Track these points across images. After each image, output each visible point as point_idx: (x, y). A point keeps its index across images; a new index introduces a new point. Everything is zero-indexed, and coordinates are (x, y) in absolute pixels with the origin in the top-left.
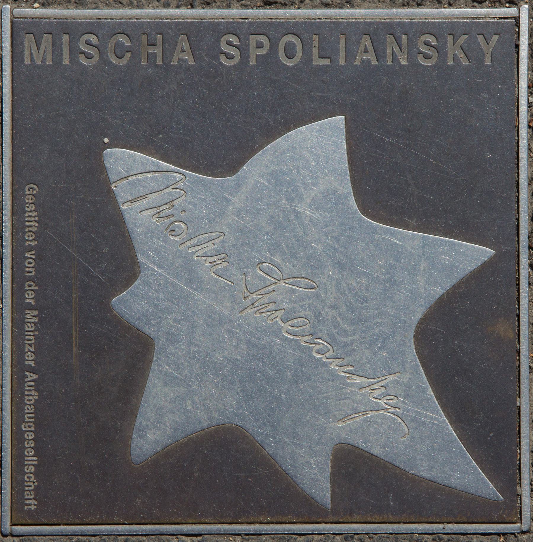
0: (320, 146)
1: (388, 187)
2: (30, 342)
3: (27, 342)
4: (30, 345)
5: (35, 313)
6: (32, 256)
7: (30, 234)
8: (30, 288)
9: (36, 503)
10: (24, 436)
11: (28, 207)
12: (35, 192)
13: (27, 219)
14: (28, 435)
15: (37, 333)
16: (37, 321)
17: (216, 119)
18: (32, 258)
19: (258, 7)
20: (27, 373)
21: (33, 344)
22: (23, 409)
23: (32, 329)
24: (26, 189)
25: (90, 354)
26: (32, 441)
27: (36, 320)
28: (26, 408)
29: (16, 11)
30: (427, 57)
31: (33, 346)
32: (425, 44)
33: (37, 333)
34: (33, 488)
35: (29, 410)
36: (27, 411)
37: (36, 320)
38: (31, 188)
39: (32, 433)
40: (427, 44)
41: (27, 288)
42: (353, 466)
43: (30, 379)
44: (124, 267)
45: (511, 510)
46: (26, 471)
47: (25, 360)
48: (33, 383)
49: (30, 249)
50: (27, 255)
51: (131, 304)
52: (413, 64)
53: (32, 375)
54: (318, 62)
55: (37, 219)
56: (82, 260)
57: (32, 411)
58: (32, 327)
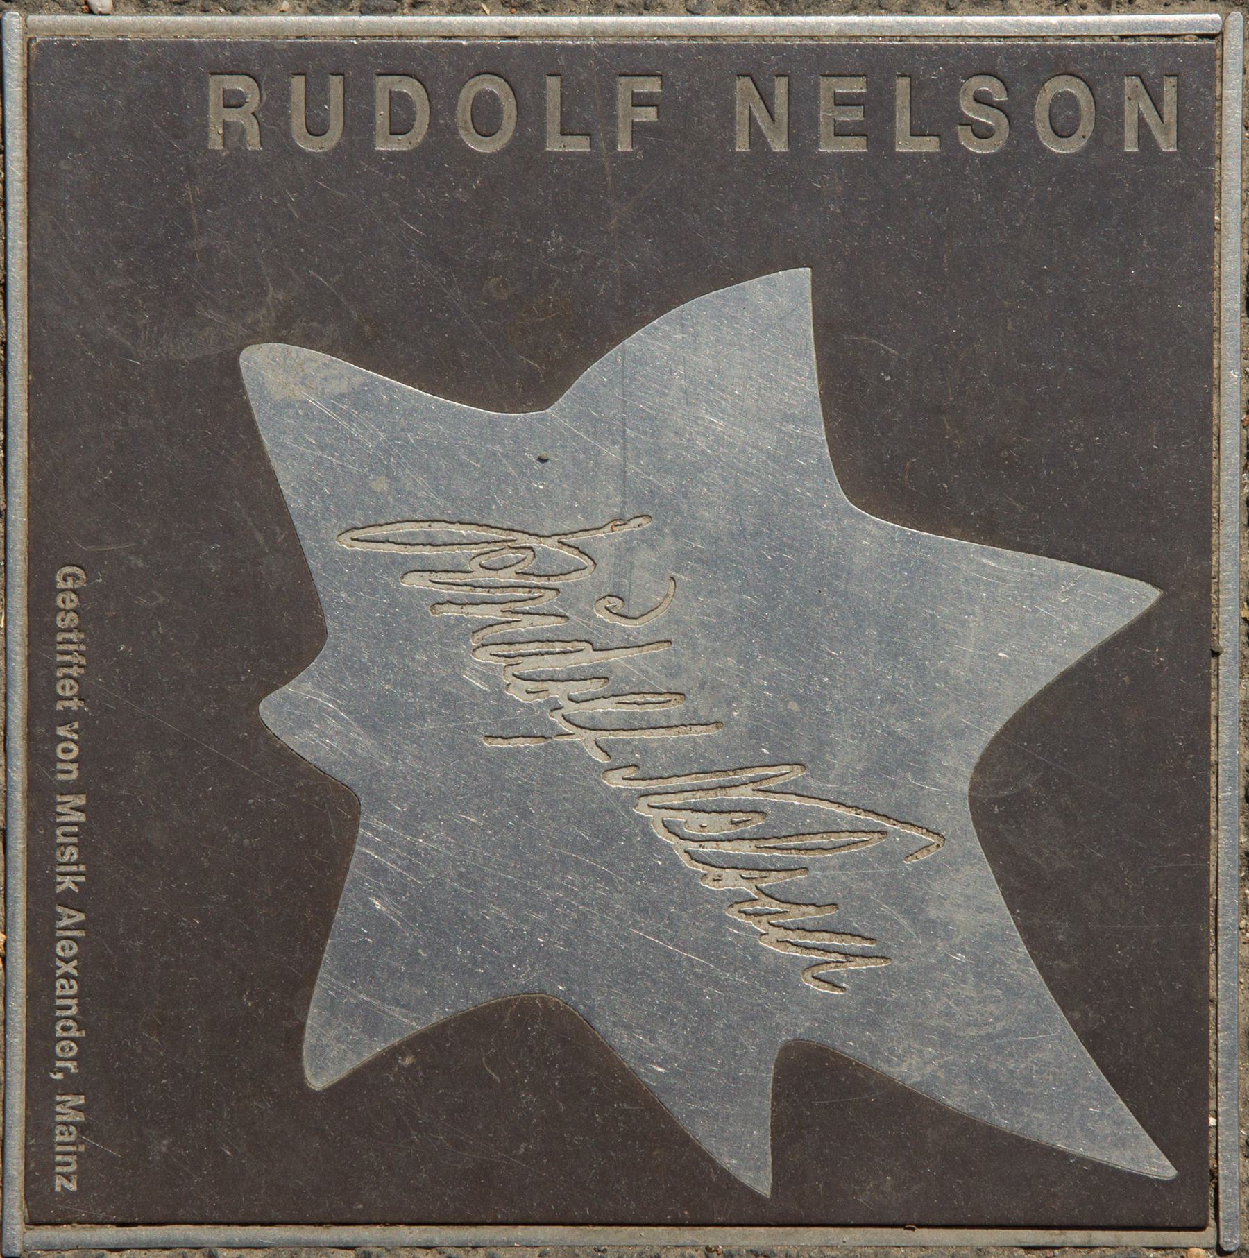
0: (734, 368)
1: (916, 442)
2: (65, 1169)
3: (58, 1169)
4: (67, 1176)
5: (81, 801)
6: (75, 737)
7: (68, 682)
8: (65, 1034)
9: (83, 662)
10: (55, 687)
11: (63, 620)
12: (80, 584)
13: (60, 647)
14: (63, 688)
15: (82, 1148)
16: (82, 1102)
17: (511, 259)
18: (73, 741)
19: (590, 14)
20: (59, 909)
21: (74, 1173)
22: (51, 1133)
23: (72, 1138)
24: (59, 578)
25: (204, 879)
26: (74, 615)
27: (80, 817)
28: (57, 1132)
29: (34, 19)
30: (983, 133)
31: (74, 1178)
32: (975, 100)
33: (82, 1148)
34: (73, 1168)
35: (66, 989)
36: (59, 1138)
37: (80, 817)
38: (70, 575)
39: (73, 596)
40: (981, 99)
41: (59, 1033)
42: (824, 1096)
43: (65, 922)
44: (285, 628)
45: (1187, 1201)
46: (60, 691)
47: (53, 998)
48: (75, 829)
49: (66, 718)
50: (62, 731)
51: (309, 717)
52: (952, 154)
53: (72, 913)
54: (905, 145)
55: (83, 648)
56: (193, 589)
57: (71, 992)
58: (71, 987)
